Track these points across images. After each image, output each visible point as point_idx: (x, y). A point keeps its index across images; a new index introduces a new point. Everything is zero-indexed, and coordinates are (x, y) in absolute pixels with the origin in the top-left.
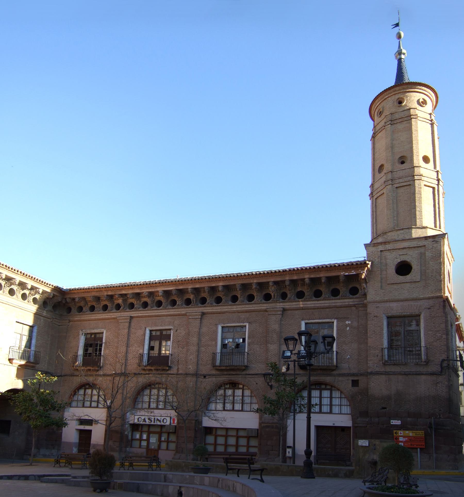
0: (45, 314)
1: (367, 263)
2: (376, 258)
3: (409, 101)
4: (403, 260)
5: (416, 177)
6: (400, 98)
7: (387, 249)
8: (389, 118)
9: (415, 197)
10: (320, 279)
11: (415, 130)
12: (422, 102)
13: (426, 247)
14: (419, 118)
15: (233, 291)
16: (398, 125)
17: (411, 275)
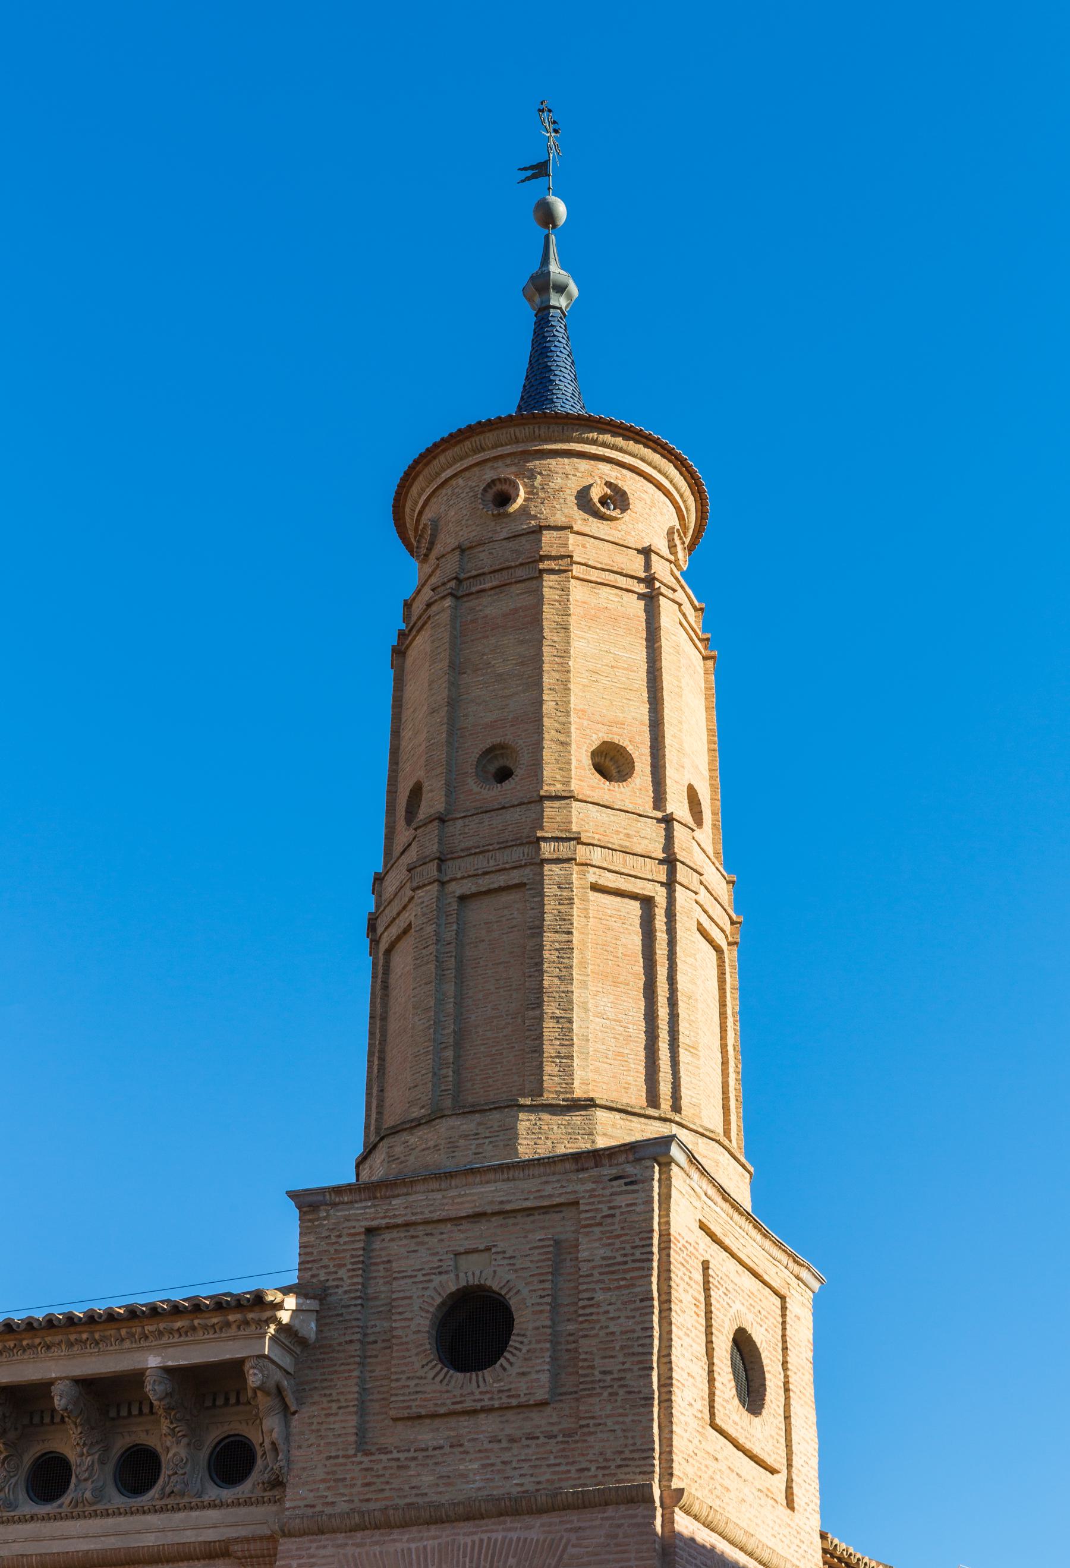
0: (427, 1479)
1: (270, 1298)
2: (342, 1273)
3: (542, 495)
4: (473, 1281)
5: (547, 850)
6: (499, 479)
7: (399, 1221)
8: (451, 565)
9: (540, 948)
10: (43, 1389)
11: (554, 625)
12: (603, 501)
13: (582, 1208)
14: (577, 570)
15: (42, 1423)
16: (485, 600)
17: (506, 1364)
